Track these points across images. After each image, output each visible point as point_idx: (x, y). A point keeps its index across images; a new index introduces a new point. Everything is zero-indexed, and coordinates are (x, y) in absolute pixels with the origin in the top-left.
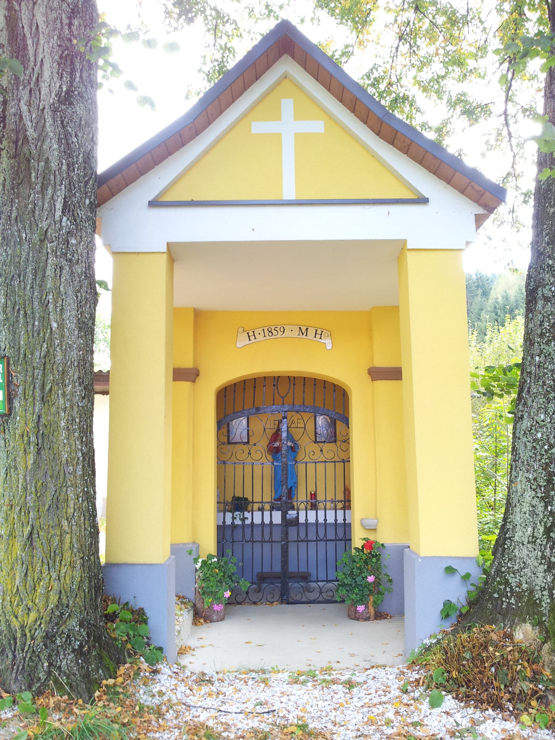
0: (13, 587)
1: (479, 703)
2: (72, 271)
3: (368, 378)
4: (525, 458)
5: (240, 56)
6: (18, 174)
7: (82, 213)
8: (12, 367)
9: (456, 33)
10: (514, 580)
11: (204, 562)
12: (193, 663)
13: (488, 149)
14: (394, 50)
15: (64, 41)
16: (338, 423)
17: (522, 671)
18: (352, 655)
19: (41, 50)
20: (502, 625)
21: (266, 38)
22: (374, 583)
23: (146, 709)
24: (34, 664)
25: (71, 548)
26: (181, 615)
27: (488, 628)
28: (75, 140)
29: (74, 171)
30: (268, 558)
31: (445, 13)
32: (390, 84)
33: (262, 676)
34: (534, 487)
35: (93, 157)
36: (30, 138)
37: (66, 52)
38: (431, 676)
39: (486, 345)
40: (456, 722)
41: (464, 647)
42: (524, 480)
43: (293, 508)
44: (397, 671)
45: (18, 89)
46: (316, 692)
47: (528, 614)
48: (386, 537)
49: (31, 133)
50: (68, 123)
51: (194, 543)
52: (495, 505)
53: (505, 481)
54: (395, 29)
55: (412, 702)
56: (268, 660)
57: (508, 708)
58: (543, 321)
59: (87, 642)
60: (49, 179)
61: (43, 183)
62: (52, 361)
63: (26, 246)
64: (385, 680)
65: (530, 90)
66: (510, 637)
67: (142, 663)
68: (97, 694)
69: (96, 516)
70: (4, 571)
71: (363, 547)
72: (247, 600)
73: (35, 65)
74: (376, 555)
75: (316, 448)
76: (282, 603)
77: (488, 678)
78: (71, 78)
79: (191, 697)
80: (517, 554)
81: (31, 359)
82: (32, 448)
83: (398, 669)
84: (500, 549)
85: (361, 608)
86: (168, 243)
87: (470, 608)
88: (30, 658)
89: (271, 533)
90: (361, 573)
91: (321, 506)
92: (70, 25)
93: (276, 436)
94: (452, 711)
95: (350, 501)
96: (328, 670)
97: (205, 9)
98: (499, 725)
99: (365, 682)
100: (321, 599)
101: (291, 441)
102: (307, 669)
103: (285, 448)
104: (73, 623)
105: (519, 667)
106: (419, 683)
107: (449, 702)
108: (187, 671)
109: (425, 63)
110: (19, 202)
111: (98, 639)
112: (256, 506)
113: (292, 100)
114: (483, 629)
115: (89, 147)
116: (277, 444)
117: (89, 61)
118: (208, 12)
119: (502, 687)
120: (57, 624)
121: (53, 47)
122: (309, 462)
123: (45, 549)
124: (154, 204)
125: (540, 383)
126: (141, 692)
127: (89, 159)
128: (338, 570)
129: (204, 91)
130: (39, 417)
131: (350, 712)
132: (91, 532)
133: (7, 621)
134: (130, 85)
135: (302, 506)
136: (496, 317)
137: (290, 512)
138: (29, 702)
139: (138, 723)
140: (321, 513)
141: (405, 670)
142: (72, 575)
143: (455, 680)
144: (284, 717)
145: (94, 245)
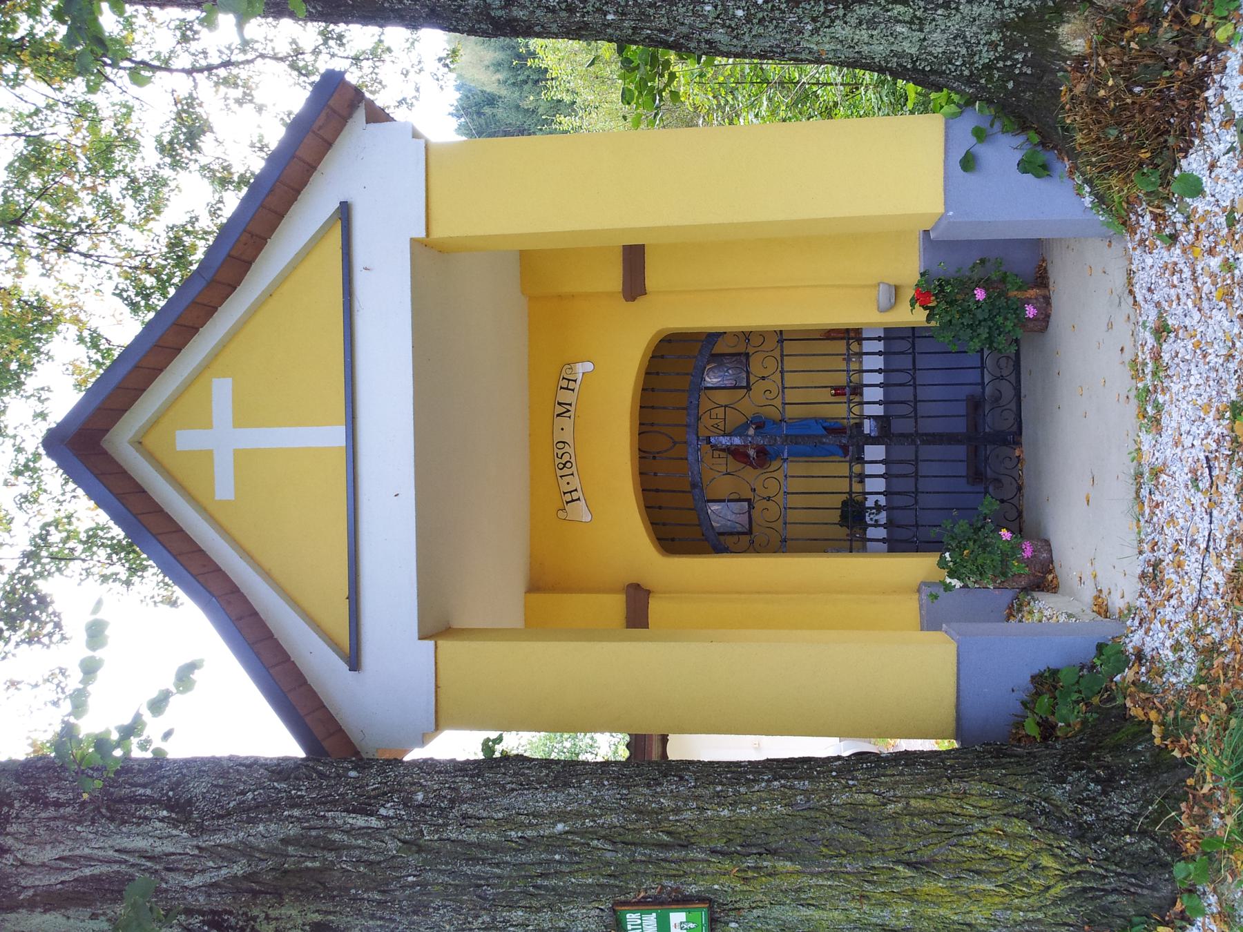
0: (997, 894)
1: (1196, 112)
2: (470, 799)
3: (641, 301)
4: (779, 37)
5: (103, 517)
6: (308, 890)
7: (373, 784)
8: (630, 897)
9: (56, 156)
10: (984, 55)
11: (952, 574)
12: (1124, 590)
13: (251, 101)
14: (89, 261)
15: (84, 815)
16: (718, 349)
17: (1141, 40)
18: (1110, 326)
19: (101, 853)
20: (1060, 74)
21: (72, 474)
22: (986, 290)
23: (1203, 673)
24: (1128, 859)
25: (932, 797)
26: (1040, 611)
27: (1065, 99)
28: (250, 796)
29: (302, 796)
30: (943, 467)
31: (25, 175)
32: (146, 268)
33: (1146, 478)
34: (827, 22)
35: (279, 765)
36: (248, 870)
37: (104, 811)
38: (1147, 194)
39: (578, 100)
40: (1228, 152)
41: (1099, 139)
42: (816, 38)
43: (859, 426)
44: (1138, 252)
45: (166, 891)
46: (1176, 388)
47: (1041, 31)
48: (908, 269)
49: (238, 869)
50: (222, 807)
51: (919, 591)
52: (849, 84)
53: (811, 69)
54: (52, 261)
55: (1192, 226)
56: (1122, 466)
57: (1204, 63)
58: (547, 8)
59: (1090, 770)
60: (316, 838)
61: (323, 849)
62: (621, 830)
63: (429, 876)
64: (1153, 271)
65: (154, 32)
66: (1080, 60)
67: (1124, 678)
68: (1177, 753)
69: (877, 756)
70: (971, 908)
71: (926, 308)
72: (1015, 501)
73: (126, 861)
74: (940, 285)
75: (759, 387)
76: (1018, 443)
77: (1151, 97)
78: (146, 802)
79: (1183, 597)
80: (940, 50)
81: (616, 866)
82: (765, 864)
83: (1134, 249)
84: (932, 78)
85: (1030, 311)
86: (420, 638)
87: (1030, 128)
88: (1116, 865)
89: (901, 462)
90: (970, 311)
91: (855, 378)
92: (57, 804)
93: (737, 454)
94: (1209, 159)
95: (847, 330)
96: (1136, 368)
97: (23, 577)
98: (1233, 80)
99: (1158, 304)
100: (1012, 378)
101: (747, 429)
102: (1134, 402)
103: (759, 439)
104: (1058, 793)
105: (1133, 45)
106: (1160, 215)
107: (1193, 163)
108: (1138, 604)
109: (111, 211)
110: (355, 888)
111: (1085, 752)
112: (857, 487)
113: (178, 432)
114: (1067, 107)
115: (262, 771)
116: (752, 452)
117: (117, 773)
118: (28, 571)
119: (1167, 73)
120: (1061, 821)
121: (96, 833)
122: (783, 398)
123: (935, 841)
124: (354, 661)
125: (652, 11)
126: (1174, 680)
127: (280, 769)
128: (966, 349)
129: (161, 576)
130: (713, 852)
131: (1210, 330)
132: (906, 765)
133: (1054, 903)
134: (158, 705)
135: (856, 410)
136: (530, 83)
137: (867, 431)
138: (1191, 866)
139: (1228, 685)
140: (868, 378)
141: (1137, 237)
142: (976, 798)
143: (1155, 153)
144: (1218, 442)
145: (425, 761)
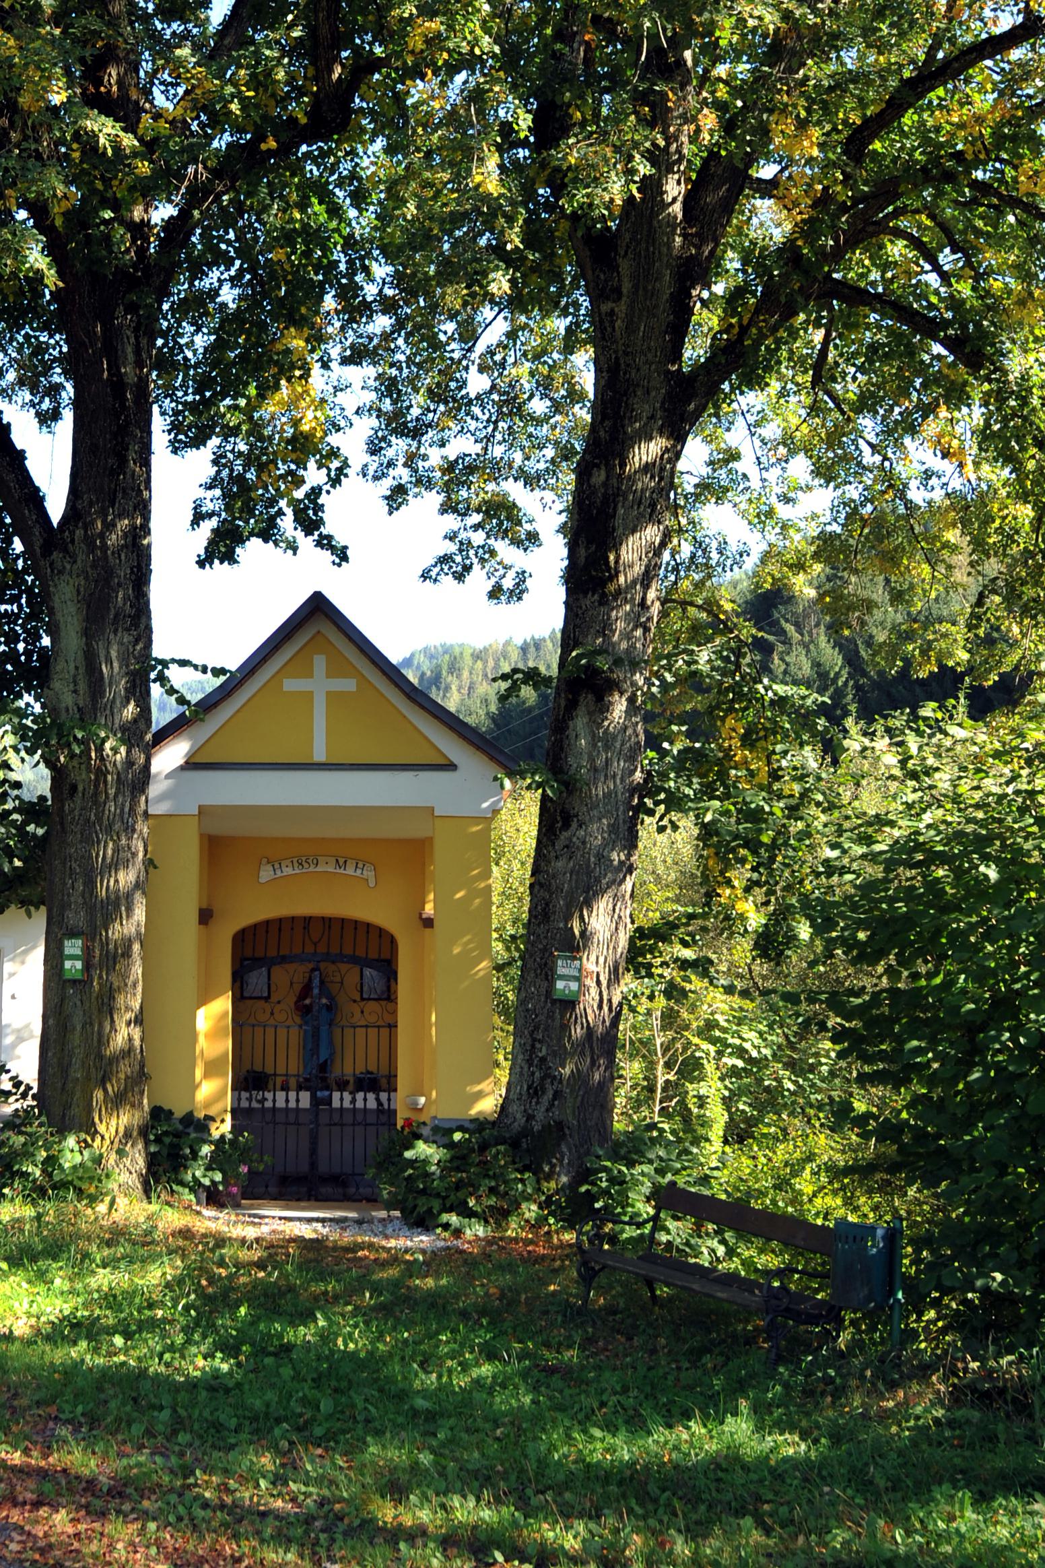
112: (279, 1080)
116: (307, 1002)
